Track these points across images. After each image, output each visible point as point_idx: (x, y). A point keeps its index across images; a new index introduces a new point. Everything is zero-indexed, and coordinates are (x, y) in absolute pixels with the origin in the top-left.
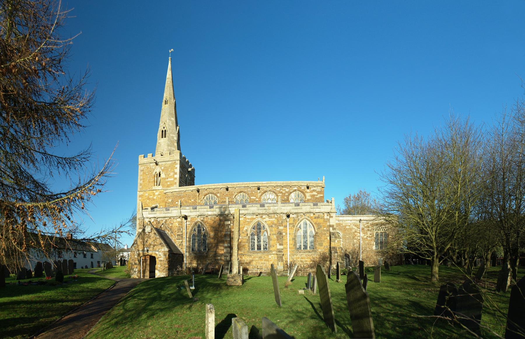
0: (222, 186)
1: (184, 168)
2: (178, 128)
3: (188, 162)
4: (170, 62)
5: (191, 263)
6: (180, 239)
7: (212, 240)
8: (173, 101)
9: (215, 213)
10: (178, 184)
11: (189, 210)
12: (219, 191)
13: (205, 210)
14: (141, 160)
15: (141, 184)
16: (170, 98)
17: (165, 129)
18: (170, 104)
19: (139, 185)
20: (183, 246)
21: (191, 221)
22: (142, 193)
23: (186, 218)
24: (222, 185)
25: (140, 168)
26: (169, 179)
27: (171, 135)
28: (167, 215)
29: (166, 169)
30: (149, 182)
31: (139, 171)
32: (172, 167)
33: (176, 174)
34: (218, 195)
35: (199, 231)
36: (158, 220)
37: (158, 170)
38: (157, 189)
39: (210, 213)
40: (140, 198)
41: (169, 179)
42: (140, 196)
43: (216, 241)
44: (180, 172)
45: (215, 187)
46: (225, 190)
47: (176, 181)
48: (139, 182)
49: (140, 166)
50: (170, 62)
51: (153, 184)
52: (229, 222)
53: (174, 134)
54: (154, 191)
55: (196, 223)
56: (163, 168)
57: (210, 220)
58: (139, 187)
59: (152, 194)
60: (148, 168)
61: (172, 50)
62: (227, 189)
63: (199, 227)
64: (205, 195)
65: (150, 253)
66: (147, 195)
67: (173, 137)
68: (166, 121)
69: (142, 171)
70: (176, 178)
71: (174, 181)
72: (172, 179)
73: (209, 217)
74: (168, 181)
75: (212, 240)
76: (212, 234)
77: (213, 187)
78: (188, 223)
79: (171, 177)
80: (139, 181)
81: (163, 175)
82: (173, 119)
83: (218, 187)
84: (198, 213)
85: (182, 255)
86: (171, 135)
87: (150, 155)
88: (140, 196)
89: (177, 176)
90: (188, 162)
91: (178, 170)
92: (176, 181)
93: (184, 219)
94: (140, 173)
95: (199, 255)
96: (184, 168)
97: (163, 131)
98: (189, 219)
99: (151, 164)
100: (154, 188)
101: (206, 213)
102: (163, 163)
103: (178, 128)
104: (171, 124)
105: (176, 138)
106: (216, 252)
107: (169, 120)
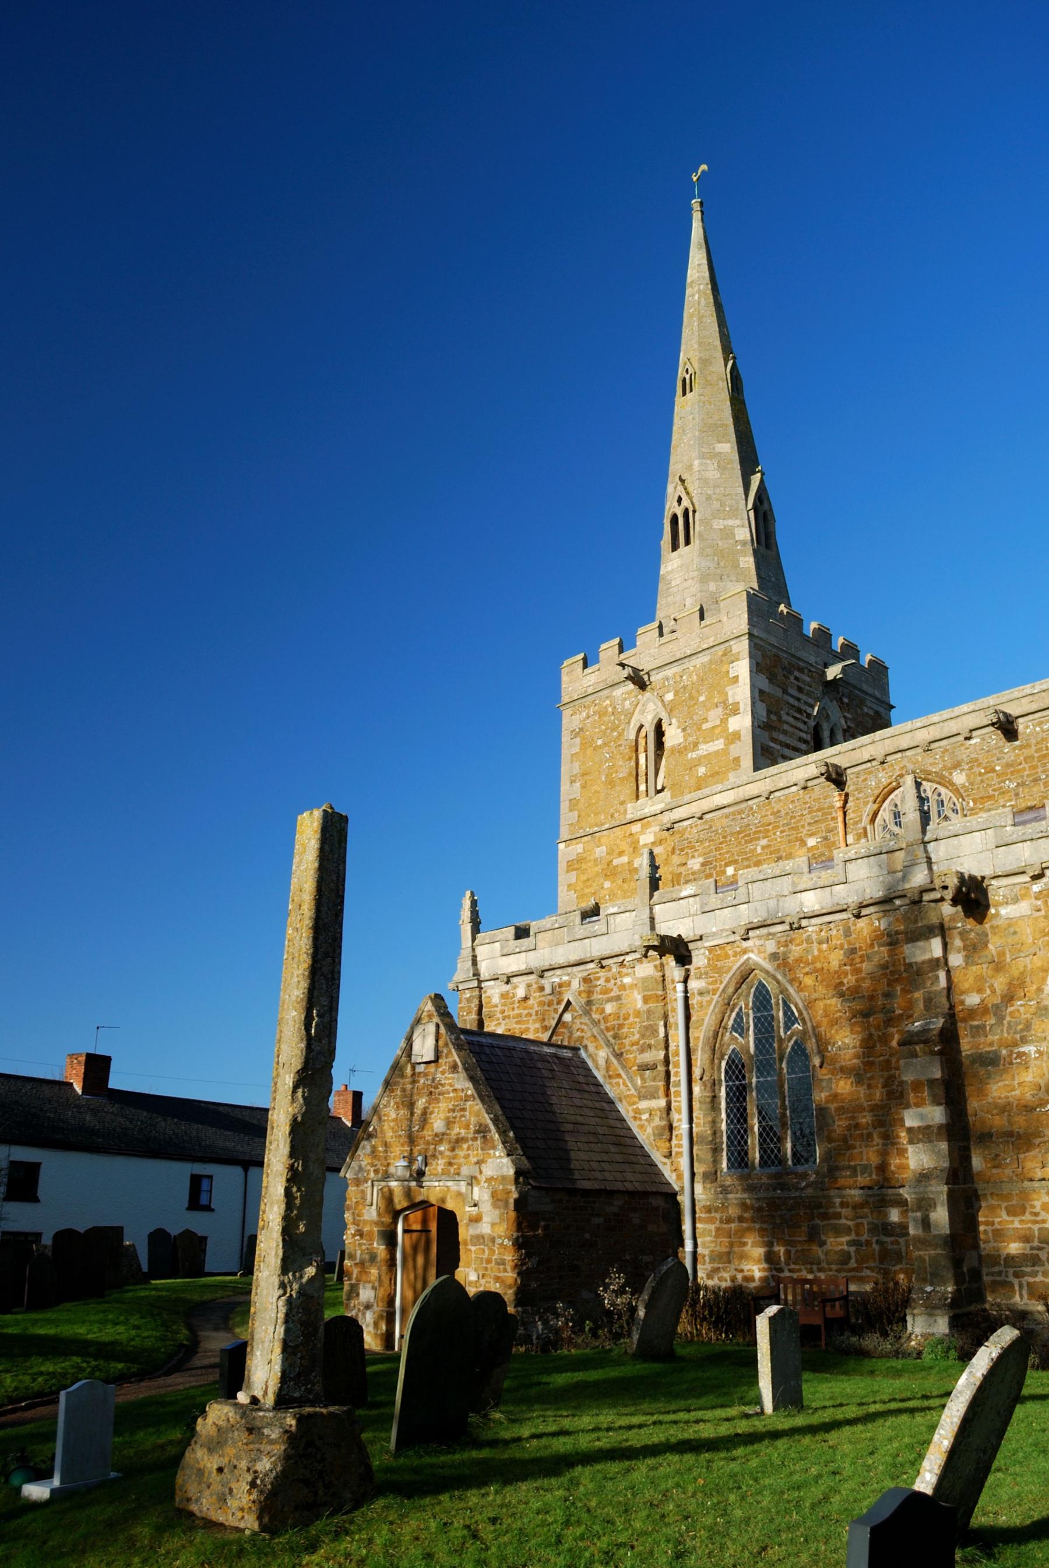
0: (972, 721)
1: (788, 670)
2: (756, 479)
3: (824, 635)
4: (697, 216)
5: (726, 1257)
6: (653, 1096)
7: (844, 1087)
8: (720, 370)
9: (847, 895)
10: (747, 761)
11: (694, 905)
12: (963, 754)
13: (785, 885)
14: (575, 679)
15: (573, 804)
16: (705, 362)
17: (686, 503)
18: (708, 383)
19: (564, 806)
20: (670, 1128)
21: (715, 968)
22: (578, 848)
23: (678, 950)
24: (972, 713)
25: (570, 721)
26: (704, 749)
27: (718, 524)
28: (597, 948)
29: (686, 702)
30: (611, 783)
31: (565, 738)
32: (716, 677)
33: (735, 711)
34: (959, 778)
35: (765, 1027)
36: (554, 977)
37: (647, 710)
38: (649, 810)
39: (811, 902)
40: (573, 877)
41: (704, 749)
42: (571, 866)
43: (878, 1094)
44: (759, 695)
45: (934, 733)
46: (996, 737)
47: (735, 750)
48: (568, 790)
49: (566, 713)
50: (697, 216)
51: (629, 788)
52: (935, 947)
53: (733, 513)
54: (636, 828)
55: (745, 976)
56: (669, 697)
57: (827, 950)
58: (567, 817)
59: (624, 846)
60: (602, 714)
61: (704, 167)
62: (1007, 728)
63: (762, 1000)
64: (882, 798)
65: (434, 1189)
66: (601, 851)
67: (728, 533)
68: (690, 467)
69: (575, 734)
70: (736, 736)
71: (725, 751)
72: (719, 745)
73: (812, 927)
74: (698, 762)
75: (844, 1087)
76: (845, 1041)
77: (923, 736)
78: (694, 984)
79: (710, 736)
80: (565, 787)
81: (673, 737)
82: (728, 448)
83: (952, 727)
84: (746, 914)
85: (672, 1197)
86: (718, 524)
87: (609, 649)
88: (571, 866)
89: (743, 723)
90: (824, 635)
91: (742, 692)
92: (735, 750)
93: (670, 961)
94: (569, 746)
95: (782, 1202)
96: (788, 670)
97: (674, 519)
98: (699, 959)
99: (618, 692)
100: (633, 810)
101: (791, 907)
102: (669, 672)
103: (756, 479)
104: (713, 474)
105: (744, 533)
106: (883, 1168)
107: (703, 456)
